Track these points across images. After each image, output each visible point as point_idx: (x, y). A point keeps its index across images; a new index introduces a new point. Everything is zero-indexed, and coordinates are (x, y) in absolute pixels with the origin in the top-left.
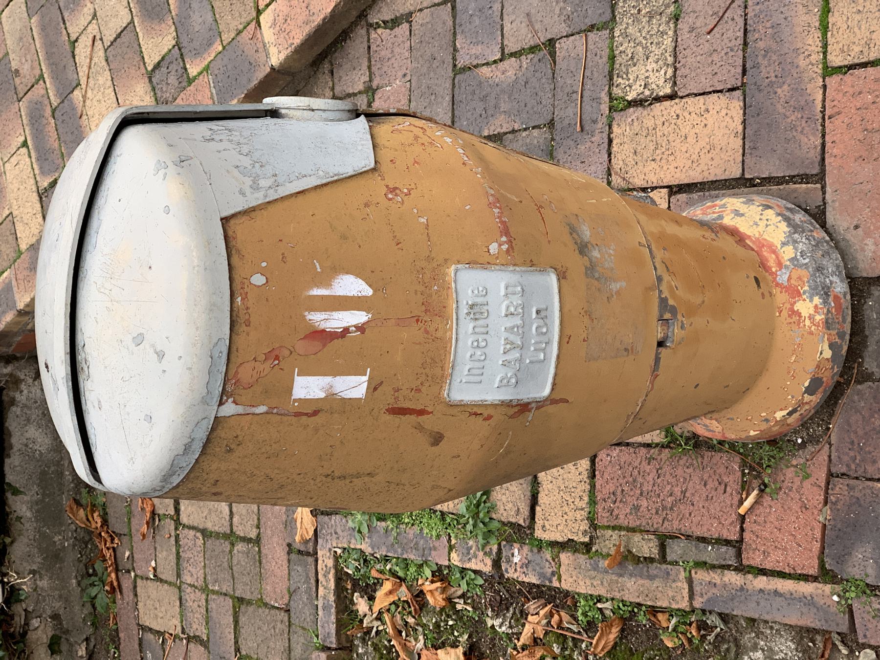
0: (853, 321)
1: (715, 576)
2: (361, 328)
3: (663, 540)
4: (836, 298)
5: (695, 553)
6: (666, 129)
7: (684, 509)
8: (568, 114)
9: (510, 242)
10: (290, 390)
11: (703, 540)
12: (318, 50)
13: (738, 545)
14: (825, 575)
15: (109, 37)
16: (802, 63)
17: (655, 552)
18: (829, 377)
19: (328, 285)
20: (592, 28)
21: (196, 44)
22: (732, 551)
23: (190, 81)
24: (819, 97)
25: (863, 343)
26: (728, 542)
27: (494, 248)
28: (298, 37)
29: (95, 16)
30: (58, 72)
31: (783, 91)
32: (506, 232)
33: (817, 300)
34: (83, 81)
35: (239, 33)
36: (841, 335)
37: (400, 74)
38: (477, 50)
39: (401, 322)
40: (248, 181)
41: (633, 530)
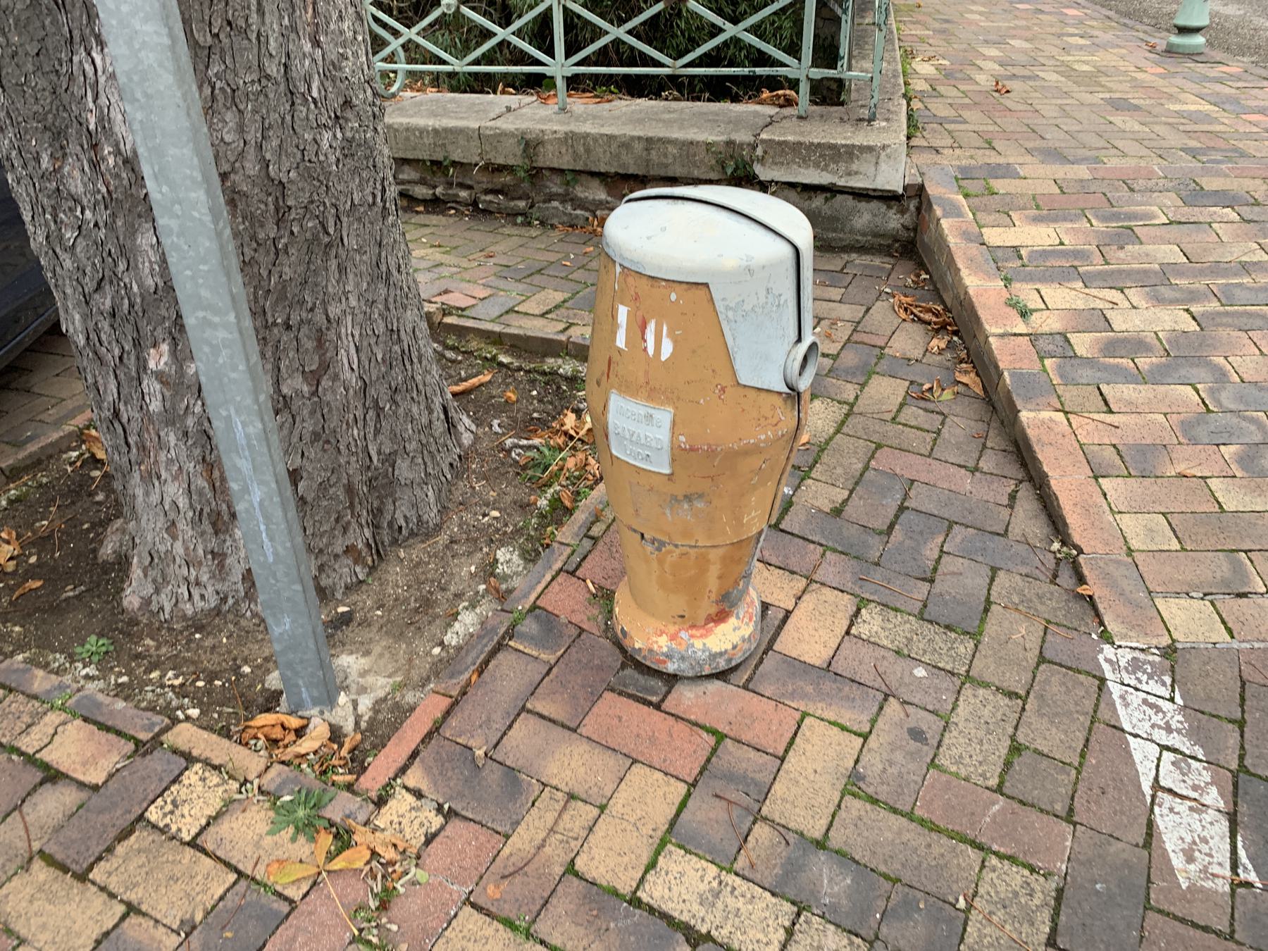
0: (649, 668)
1: (564, 557)
2: (645, 349)
3: (595, 540)
4: (665, 662)
5: (581, 551)
6: (829, 622)
7: (605, 555)
8: (877, 575)
9: (685, 450)
10: (622, 303)
11: (584, 558)
12: (1021, 443)
13: (573, 573)
14: (534, 607)
15: (1109, 314)
16: (820, 705)
17: (591, 533)
18: (626, 643)
19: (669, 335)
20: (925, 606)
21: (1068, 368)
22: (571, 569)
23: (1041, 359)
24: (793, 705)
25: (642, 673)
26: (577, 569)
27: (682, 438)
28: (1031, 433)
29: (1134, 307)
30: (1101, 275)
31: (810, 689)
32: (692, 449)
33: (665, 649)
34: (1087, 291)
35: (1059, 397)
36: (644, 657)
37: (974, 491)
38: (958, 539)
39: (647, 373)
40: (732, 305)
41: (608, 527)
